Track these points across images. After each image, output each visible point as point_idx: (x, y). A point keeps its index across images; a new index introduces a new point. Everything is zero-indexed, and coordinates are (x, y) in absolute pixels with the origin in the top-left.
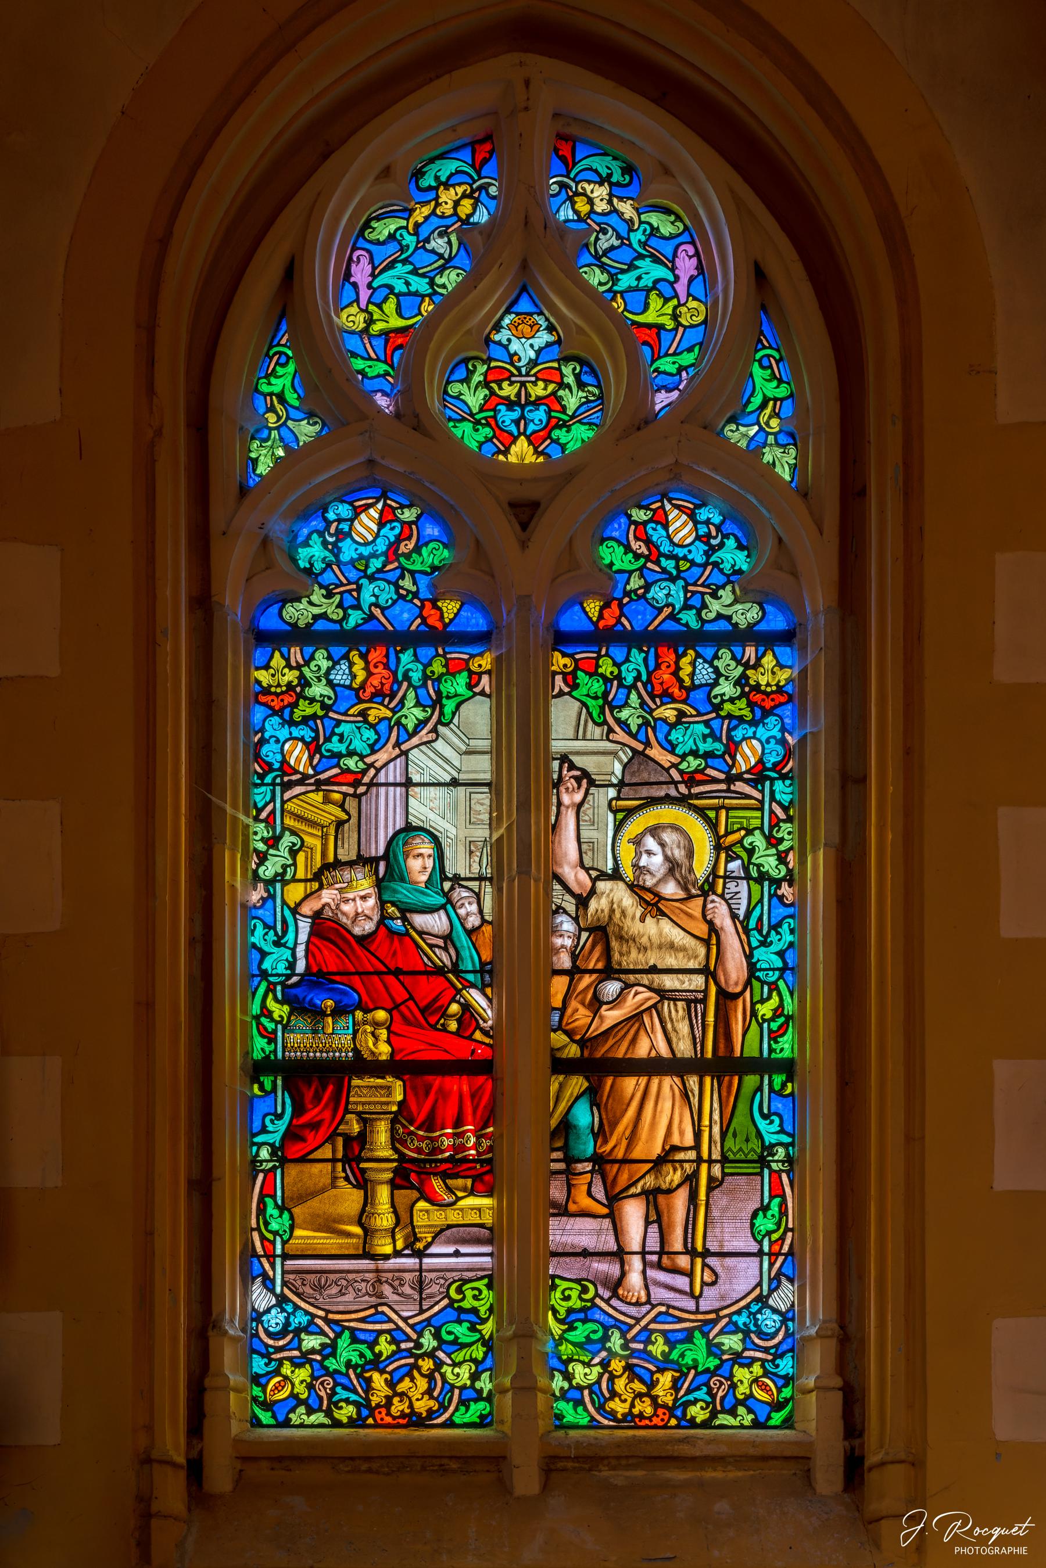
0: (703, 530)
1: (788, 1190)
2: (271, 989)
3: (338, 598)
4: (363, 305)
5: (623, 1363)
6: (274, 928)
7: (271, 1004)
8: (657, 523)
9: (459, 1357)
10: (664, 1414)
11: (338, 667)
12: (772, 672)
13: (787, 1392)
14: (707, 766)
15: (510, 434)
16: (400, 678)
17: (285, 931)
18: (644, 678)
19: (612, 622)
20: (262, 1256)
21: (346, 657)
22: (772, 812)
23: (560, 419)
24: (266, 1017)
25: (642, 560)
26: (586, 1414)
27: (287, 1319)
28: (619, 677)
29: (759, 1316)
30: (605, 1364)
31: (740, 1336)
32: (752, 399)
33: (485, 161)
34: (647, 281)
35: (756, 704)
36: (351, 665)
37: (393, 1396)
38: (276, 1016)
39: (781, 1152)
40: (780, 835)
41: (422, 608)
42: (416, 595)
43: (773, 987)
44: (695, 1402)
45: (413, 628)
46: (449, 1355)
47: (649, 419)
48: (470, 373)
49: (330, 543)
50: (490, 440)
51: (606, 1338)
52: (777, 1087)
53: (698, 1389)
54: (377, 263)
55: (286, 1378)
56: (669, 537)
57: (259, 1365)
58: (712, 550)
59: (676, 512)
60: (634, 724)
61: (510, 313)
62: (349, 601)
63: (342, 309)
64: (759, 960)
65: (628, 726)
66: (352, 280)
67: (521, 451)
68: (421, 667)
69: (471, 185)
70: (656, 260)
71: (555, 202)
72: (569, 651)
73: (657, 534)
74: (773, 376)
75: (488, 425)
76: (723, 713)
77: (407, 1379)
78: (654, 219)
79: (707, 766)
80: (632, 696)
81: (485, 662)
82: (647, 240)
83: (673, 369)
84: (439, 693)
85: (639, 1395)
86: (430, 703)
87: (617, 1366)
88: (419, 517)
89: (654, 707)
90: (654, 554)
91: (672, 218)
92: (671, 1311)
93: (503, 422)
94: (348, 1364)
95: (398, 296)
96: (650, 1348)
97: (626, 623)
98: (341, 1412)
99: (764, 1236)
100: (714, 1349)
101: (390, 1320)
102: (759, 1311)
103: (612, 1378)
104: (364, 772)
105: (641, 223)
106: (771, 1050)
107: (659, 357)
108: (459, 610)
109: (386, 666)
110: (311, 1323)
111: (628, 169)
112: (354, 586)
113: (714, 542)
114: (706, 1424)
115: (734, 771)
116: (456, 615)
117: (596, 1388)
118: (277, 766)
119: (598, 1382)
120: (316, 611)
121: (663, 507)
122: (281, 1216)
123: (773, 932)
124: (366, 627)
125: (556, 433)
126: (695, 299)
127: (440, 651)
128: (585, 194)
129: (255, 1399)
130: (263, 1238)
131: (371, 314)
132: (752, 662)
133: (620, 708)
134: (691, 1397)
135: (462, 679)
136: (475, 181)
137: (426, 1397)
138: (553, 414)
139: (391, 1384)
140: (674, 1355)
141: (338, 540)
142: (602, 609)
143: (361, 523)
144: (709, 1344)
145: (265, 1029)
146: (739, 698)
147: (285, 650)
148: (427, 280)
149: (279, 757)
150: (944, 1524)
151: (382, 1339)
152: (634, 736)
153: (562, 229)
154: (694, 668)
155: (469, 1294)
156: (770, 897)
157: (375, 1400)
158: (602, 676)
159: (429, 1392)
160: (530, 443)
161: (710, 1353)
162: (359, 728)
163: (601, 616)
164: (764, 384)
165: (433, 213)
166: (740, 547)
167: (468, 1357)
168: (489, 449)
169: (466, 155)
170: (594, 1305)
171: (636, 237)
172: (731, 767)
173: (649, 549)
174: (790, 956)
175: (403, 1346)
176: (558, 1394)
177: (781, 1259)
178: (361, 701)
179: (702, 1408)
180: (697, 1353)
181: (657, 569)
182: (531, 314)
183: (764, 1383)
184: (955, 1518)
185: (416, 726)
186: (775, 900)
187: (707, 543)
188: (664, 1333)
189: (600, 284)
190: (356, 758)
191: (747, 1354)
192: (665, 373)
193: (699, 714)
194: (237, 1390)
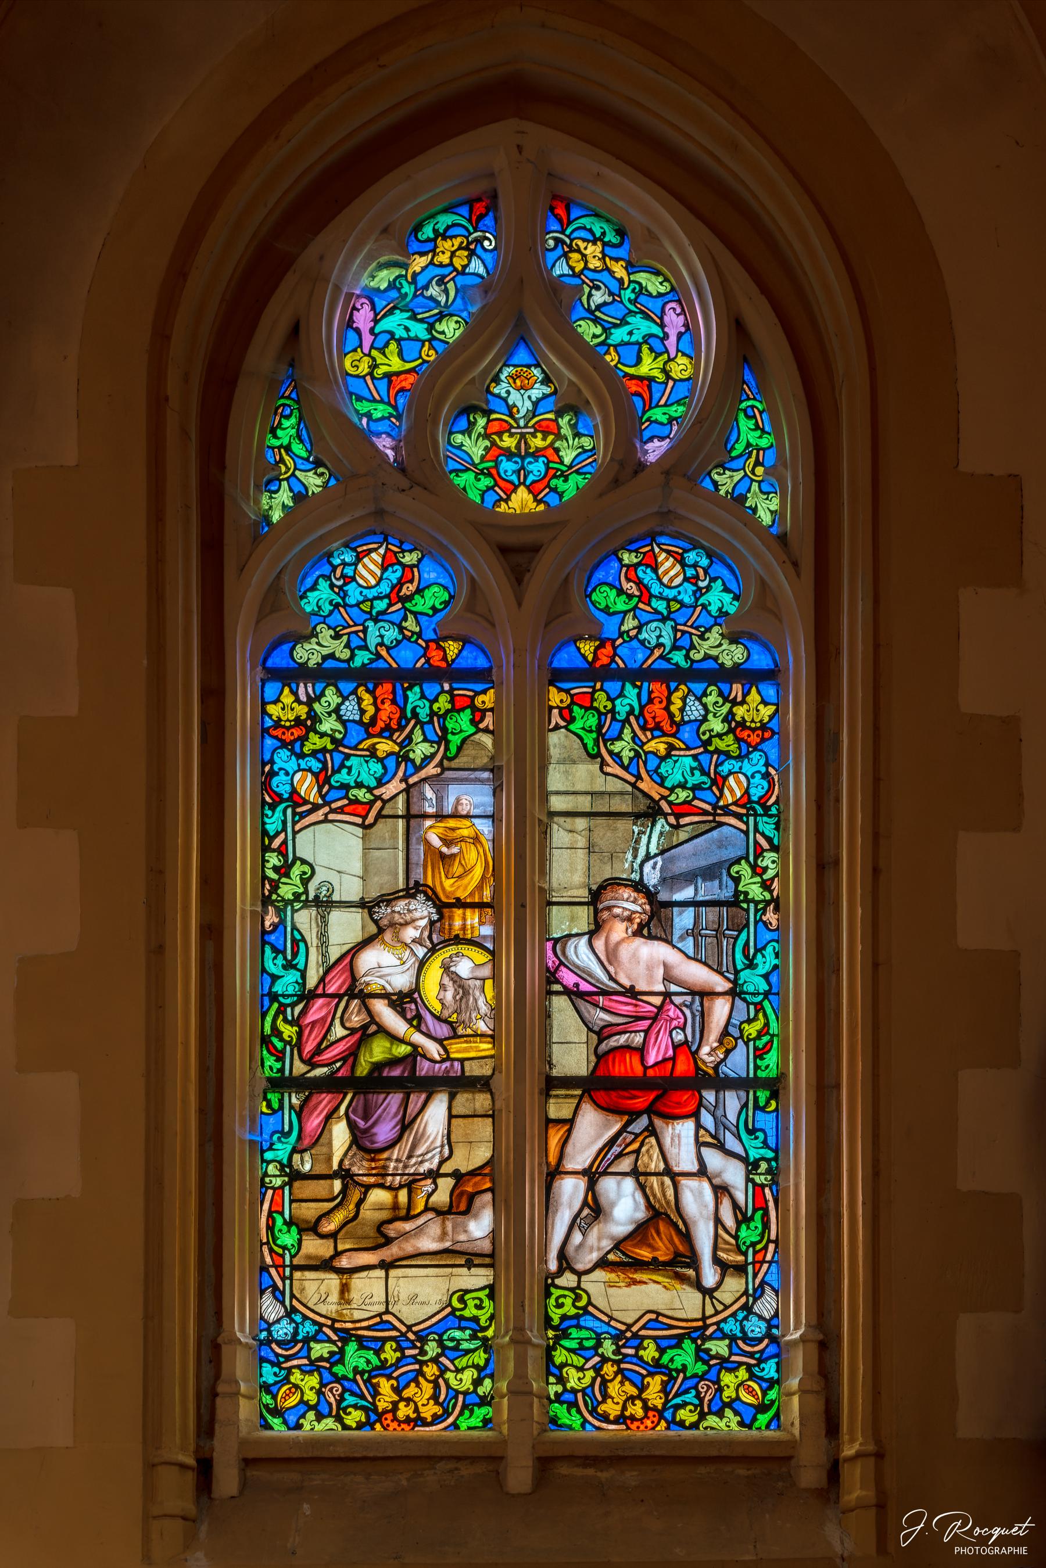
0: (690, 572)
1: (771, 1204)
2: (281, 1010)
3: (345, 638)
4: (366, 351)
5: (615, 1368)
6: (284, 952)
7: (282, 1026)
8: (647, 566)
9: (461, 1363)
10: (654, 1416)
11: (347, 703)
12: (755, 709)
13: (772, 1395)
14: (695, 798)
15: (511, 482)
16: (409, 715)
17: (295, 954)
18: (637, 712)
19: (605, 660)
20: (271, 1266)
21: (354, 692)
22: (756, 842)
23: (558, 470)
24: (276, 1037)
25: (636, 599)
26: (579, 1416)
27: (296, 1329)
28: (613, 711)
29: (745, 1322)
30: (598, 1369)
31: (727, 1342)
32: (737, 446)
33: (481, 217)
34: (637, 337)
35: (743, 740)
36: (360, 700)
37: (399, 1401)
38: (285, 1036)
39: (764, 1166)
40: (764, 864)
41: (426, 649)
42: (419, 635)
43: (759, 1007)
44: (685, 1404)
45: (419, 665)
46: (452, 1361)
47: (641, 466)
48: (472, 425)
49: (337, 587)
50: (492, 488)
51: (599, 1344)
52: (762, 1103)
53: (686, 1392)
54: (378, 311)
55: (296, 1387)
56: (659, 579)
57: (269, 1373)
58: (699, 593)
59: (664, 555)
60: (627, 755)
61: (509, 366)
62: (356, 642)
63: (346, 355)
64: (745, 982)
65: (621, 758)
66: (355, 325)
67: (521, 501)
68: (427, 704)
69: (467, 238)
70: (647, 317)
71: (551, 256)
72: (566, 685)
73: (646, 576)
74: (757, 427)
75: (490, 475)
76: (711, 748)
77: (413, 1385)
78: (642, 277)
79: (695, 798)
80: (625, 731)
81: (487, 700)
82: (636, 298)
83: (664, 419)
84: (444, 729)
85: (632, 1398)
86: (436, 739)
87: (609, 1369)
88: (420, 561)
89: (645, 740)
90: (645, 594)
91: (661, 279)
92: (661, 1318)
93: (506, 471)
94: (356, 1371)
95: (399, 341)
96: (641, 1353)
97: (620, 662)
98: (349, 1417)
99: (748, 1248)
100: (702, 1354)
101: (395, 1328)
102: (746, 1318)
103: (604, 1383)
104: (371, 803)
105: (630, 282)
106: (757, 1067)
107: (651, 408)
108: (460, 651)
109: (394, 702)
110: (317, 1332)
111: (621, 232)
112: (361, 628)
113: (701, 584)
114: (695, 1426)
115: (721, 803)
116: (458, 655)
117: (589, 1391)
118: (286, 796)
119: (592, 1385)
120: (325, 652)
121: (652, 550)
122: (289, 1231)
123: (759, 956)
124: (374, 665)
125: (554, 483)
126: (684, 354)
127: (446, 687)
128: (578, 251)
129: (266, 1406)
130: (271, 1251)
131: (374, 359)
132: (739, 699)
133: (613, 740)
134: (678, 1401)
135: (466, 715)
136: (470, 234)
137: (432, 1402)
138: (551, 465)
139: (397, 1390)
140: (665, 1359)
141: (345, 584)
142: (597, 649)
143: (365, 566)
144: (698, 1349)
145: (275, 1048)
146: (726, 734)
147: (294, 686)
148: (426, 326)
149: (288, 788)
150: (944, 1524)
151: (387, 1346)
152: (626, 768)
153: (555, 287)
154: (685, 704)
155: (471, 1304)
156: (756, 923)
157: (382, 1405)
158: (597, 710)
159: (435, 1397)
160: (530, 492)
161: (698, 1358)
162: (367, 762)
163: (596, 657)
164: (746, 432)
165: (431, 263)
166: (726, 590)
167: (470, 1363)
168: (490, 498)
169: (464, 211)
170: (586, 1312)
171: (628, 294)
172: (719, 799)
173: (640, 590)
174: (774, 979)
175: (408, 1352)
176: (552, 1397)
177: (765, 1266)
178: (370, 736)
179: (691, 1411)
180: (684, 1357)
181: (648, 609)
182: (529, 366)
183: (749, 1386)
184: (956, 1518)
185: (423, 760)
186: (760, 924)
187: (695, 584)
188: (654, 1338)
189: (595, 336)
190: (364, 790)
191: (734, 1358)
192: (656, 422)
193: (688, 748)
194: (250, 1398)
